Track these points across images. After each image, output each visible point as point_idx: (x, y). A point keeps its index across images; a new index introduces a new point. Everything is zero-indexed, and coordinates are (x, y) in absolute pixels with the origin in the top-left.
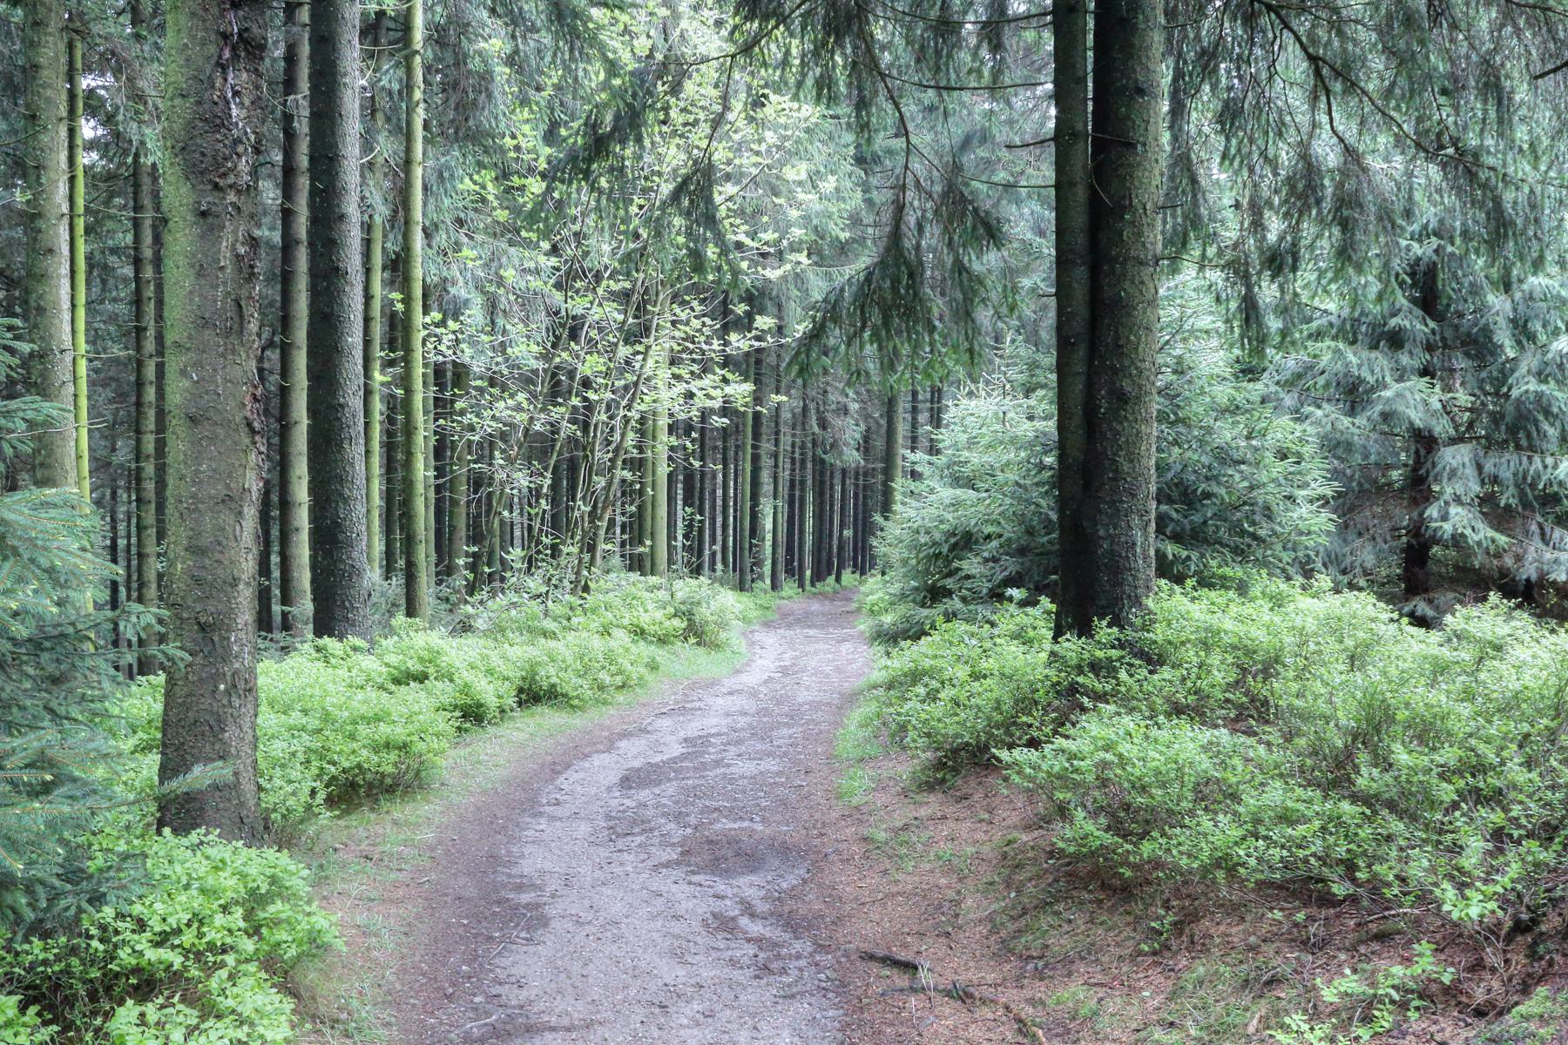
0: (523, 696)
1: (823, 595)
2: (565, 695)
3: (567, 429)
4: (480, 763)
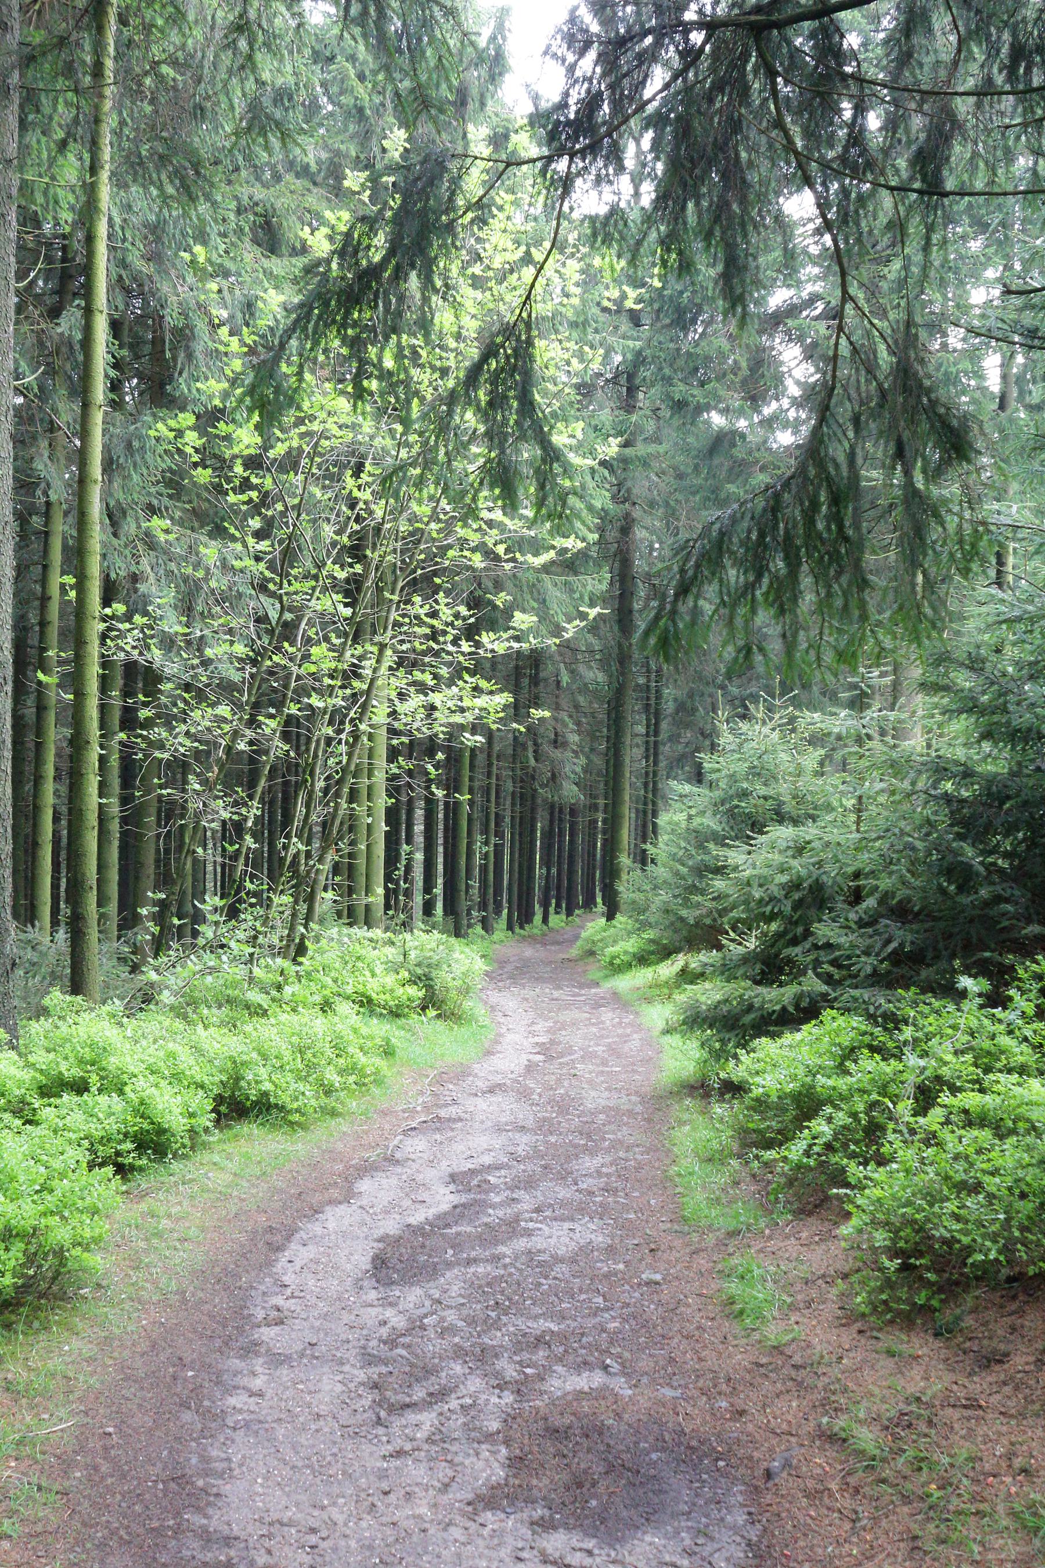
0: (223, 1109)
1: (532, 938)
2: (281, 1108)
3: (279, 747)
4: (159, 1235)
